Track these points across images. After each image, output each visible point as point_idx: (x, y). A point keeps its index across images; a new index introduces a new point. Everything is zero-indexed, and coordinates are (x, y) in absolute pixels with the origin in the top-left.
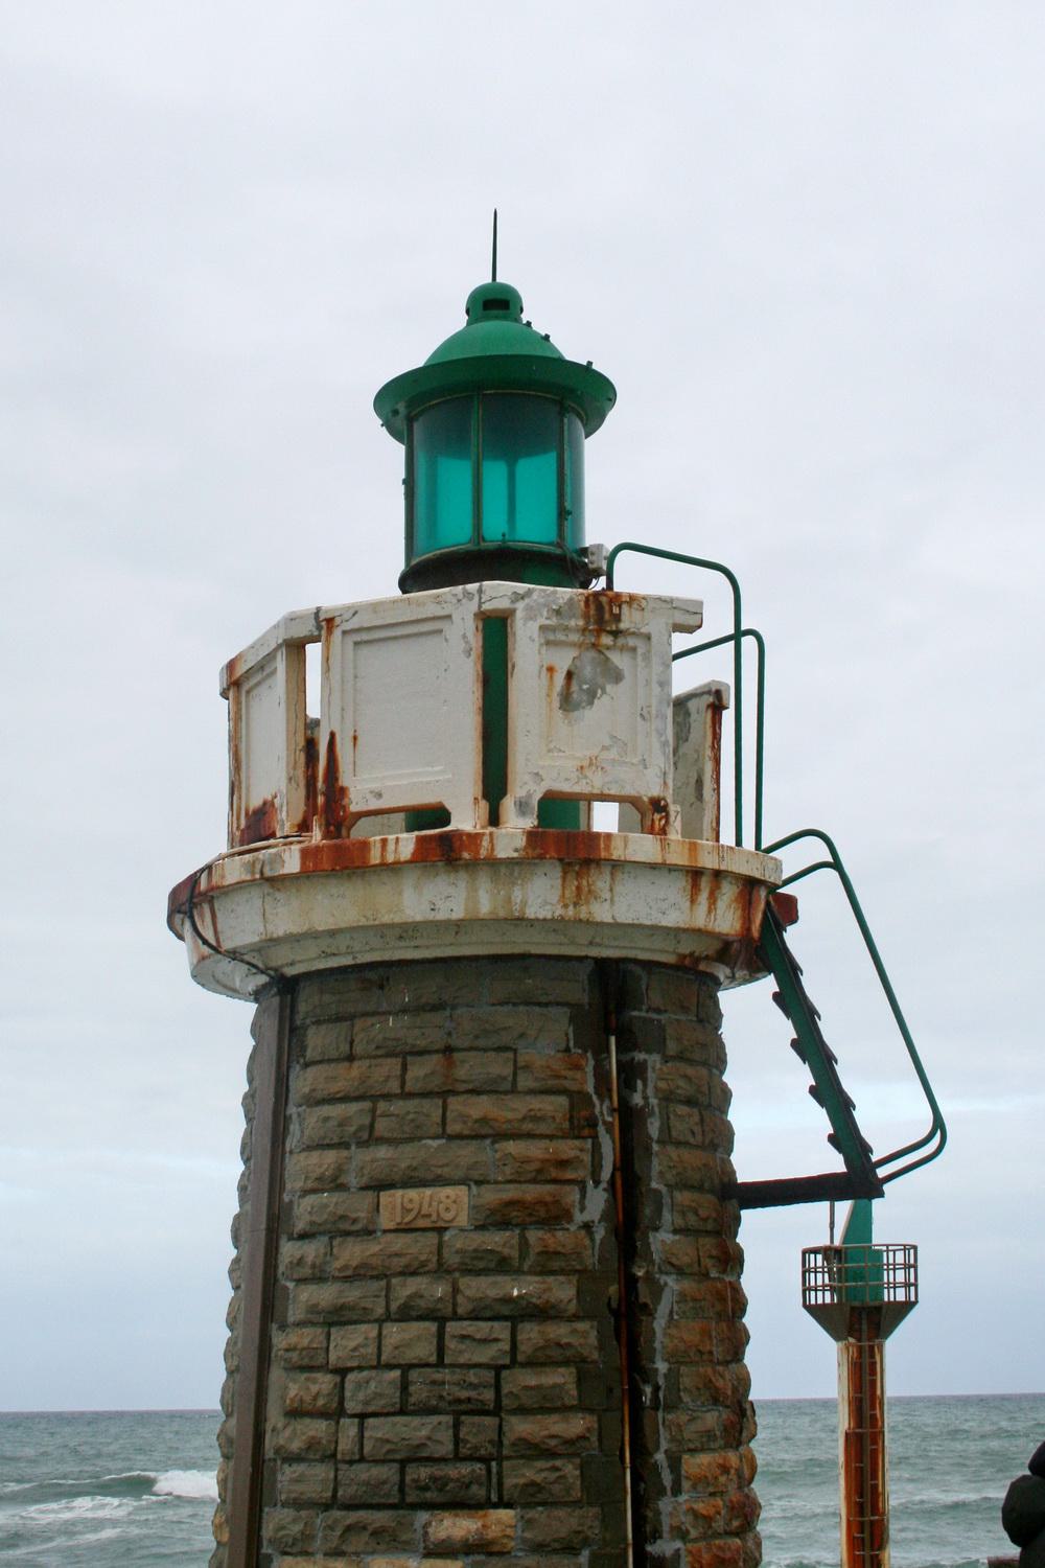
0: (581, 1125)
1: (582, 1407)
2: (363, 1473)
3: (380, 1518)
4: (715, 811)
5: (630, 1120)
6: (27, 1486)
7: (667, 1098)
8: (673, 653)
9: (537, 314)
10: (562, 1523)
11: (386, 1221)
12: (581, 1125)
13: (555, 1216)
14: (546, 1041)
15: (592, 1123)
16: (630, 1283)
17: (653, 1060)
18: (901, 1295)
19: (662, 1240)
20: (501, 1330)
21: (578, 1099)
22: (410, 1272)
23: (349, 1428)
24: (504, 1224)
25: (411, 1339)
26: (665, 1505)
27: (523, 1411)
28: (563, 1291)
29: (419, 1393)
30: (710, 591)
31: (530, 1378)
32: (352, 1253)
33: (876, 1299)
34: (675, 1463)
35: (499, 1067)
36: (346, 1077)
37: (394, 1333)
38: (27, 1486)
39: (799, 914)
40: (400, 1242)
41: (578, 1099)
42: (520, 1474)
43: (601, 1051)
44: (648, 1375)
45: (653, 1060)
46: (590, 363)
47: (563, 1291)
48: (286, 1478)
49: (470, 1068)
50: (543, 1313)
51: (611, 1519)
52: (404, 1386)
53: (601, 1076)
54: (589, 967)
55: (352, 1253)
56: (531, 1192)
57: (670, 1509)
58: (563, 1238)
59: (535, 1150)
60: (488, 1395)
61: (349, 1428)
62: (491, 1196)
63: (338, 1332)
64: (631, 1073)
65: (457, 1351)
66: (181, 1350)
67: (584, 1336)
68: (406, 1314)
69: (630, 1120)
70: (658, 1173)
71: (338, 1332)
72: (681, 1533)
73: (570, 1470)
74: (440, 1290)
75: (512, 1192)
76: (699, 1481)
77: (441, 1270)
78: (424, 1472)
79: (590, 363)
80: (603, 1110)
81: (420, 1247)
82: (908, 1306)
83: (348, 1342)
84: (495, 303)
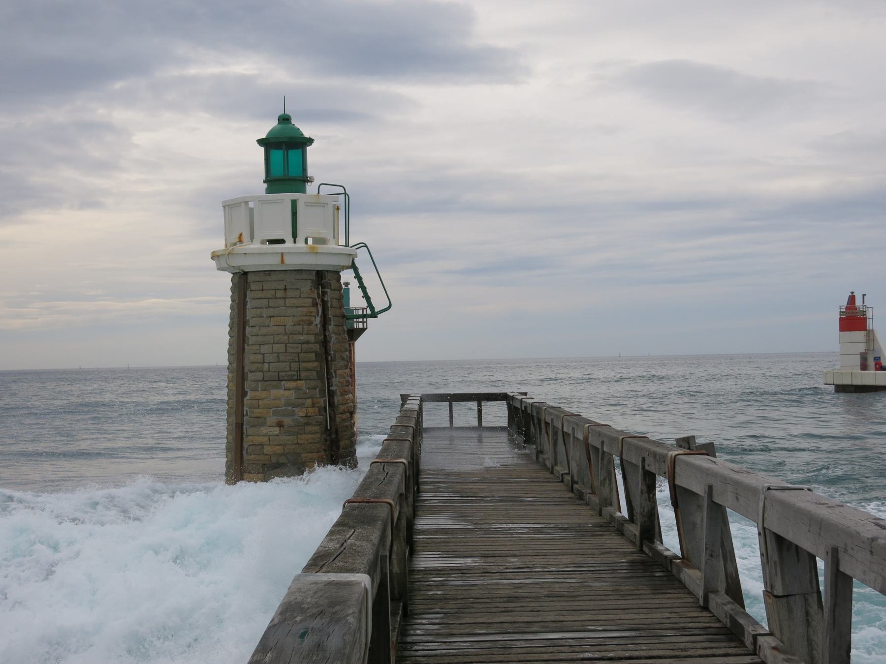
0: (315, 304)
1: (316, 361)
3: (275, 383)
4: (766, 515)
5: (324, 303)
7: (332, 298)
8: (858, 589)
10: (313, 383)
11: (271, 324)
12: (315, 304)
13: (310, 323)
14: (306, 287)
15: (317, 304)
16: (325, 336)
17: (329, 290)
18: (361, 325)
19: (331, 328)
20: (299, 346)
21: (314, 299)
23: (266, 365)
24: (299, 325)
25: (279, 348)
26: (334, 380)
27: (304, 362)
28: (312, 338)
29: (281, 358)
31: (305, 355)
32: (264, 330)
34: (335, 372)
35: (297, 293)
37: (276, 347)
40: (275, 328)
41: (314, 299)
42: (303, 374)
43: (318, 289)
44: (329, 355)
45: (329, 290)
47: (312, 338)
48: (250, 376)
49: (290, 293)
50: (308, 342)
51: (323, 382)
52: (278, 357)
53: (318, 294)
54: (314, 273)
55: (264, 330)
56: (305, 318)
57: (335, 381)
58: (312, 327)
59: (305, 310)
61: (266, 365)
62: (296, 319)
64: (324, 293)
65: (290, 350)
66: (213, 346)
67: (317, 347)
69: (324, 303)
70: (331, 313)
72: (336, 385)
73: (315, 373)
74: (286, 337)
75: (301, 318)
76: (340, 375)
77: (286, 334)
78: (283, 374)
80: (319, 301)
81: (281, 329)
82: (364, 330)
83: (264, 349)
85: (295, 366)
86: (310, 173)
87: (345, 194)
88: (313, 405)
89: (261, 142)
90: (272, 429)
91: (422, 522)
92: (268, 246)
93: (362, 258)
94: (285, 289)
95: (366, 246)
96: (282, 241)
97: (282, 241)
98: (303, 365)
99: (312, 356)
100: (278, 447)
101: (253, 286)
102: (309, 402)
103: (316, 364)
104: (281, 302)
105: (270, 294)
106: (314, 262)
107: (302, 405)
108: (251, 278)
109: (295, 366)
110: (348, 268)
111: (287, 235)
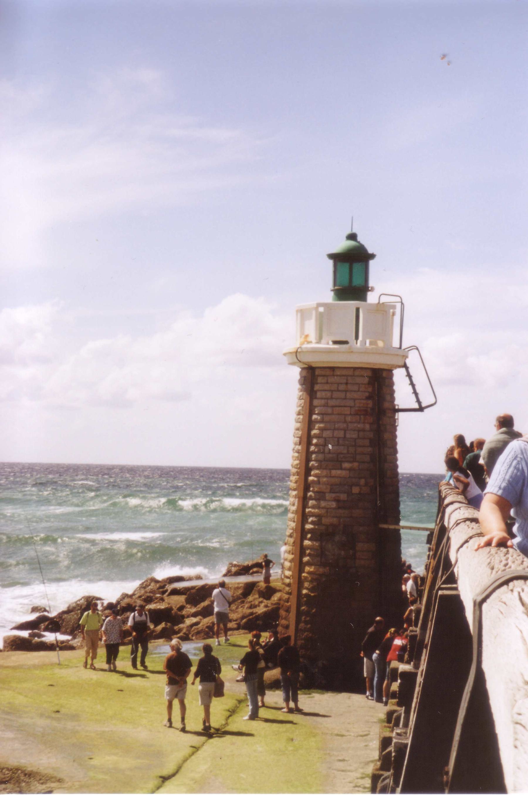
2: (331, 455)
6: (376, 675)
9: (360, 239)
22: (338, 422)
27: (360, 446)
30: (398, 299)
33: (404, 517)
36: (327, 387)
38: (376, 675)
39: (399, 447)
46: (372, 256)
50: (364, 430)
60: (354, 443)
63: (374, 757)
65: (348, 436)
67: (371, 435)
68: (338, 429)
71: (374, 757)
78: (342, 456)
79: (372, 256)
84: (352, 237)
85: (352, 450)
86: (371, 284)
87: (402, 303)
88: (366, 484)
89: (332, 256)
90: (330, 503)
91: (317, 544)
92: (336, 346)
93: (412, 360)
94: (347, 384)
95: (417, 349)
96: (346, 342)
97: (346, 342)
98: (359, 450)
99: (367, 442)
100: (335, 519)
101: (320, 380)
102: (362, 482)
103: (370, 449)
104: (342, 395)
105: (334, 387)
106: (325, 360)
107: (357, 485)
108: (317, 372)
109: (352, 450)
110: (400, 367)
111: (351, 338)
